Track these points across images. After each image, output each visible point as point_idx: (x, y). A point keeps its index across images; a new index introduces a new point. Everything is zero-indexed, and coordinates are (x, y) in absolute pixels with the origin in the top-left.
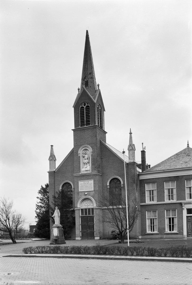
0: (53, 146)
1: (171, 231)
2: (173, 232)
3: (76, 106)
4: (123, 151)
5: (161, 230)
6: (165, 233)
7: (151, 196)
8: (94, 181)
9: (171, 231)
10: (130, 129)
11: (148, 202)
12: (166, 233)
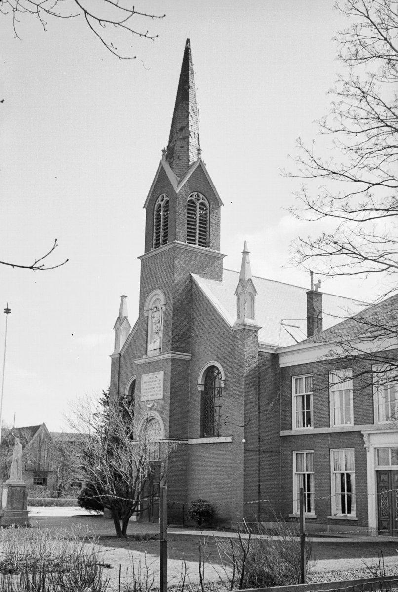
0: (126, 297)
1: (345, 513)
2: (349, 515)
3: (150, 205)
4: (6, 308)
5: (324, 508)
6: (329, 517)
7: (305, 411)
8: (165, 374)
9: (344, 514)
10: (245, 241)
11: (298, 428)
12: (332, 517)
